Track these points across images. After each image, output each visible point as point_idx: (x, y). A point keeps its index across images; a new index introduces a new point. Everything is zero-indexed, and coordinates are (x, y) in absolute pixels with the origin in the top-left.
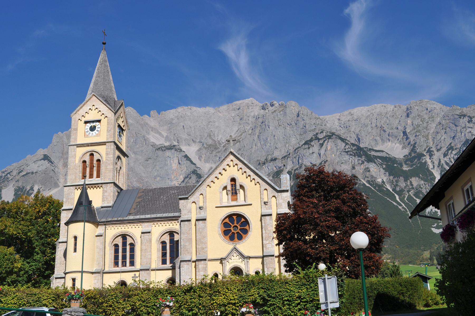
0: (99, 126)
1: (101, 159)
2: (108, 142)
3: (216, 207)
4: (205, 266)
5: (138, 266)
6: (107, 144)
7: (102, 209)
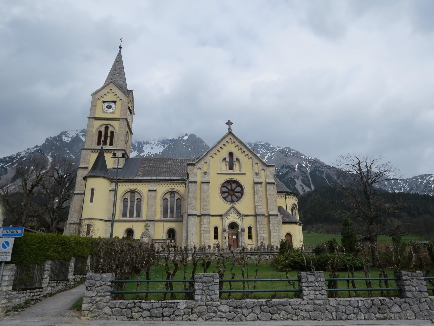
0: (114, 106)
1: (114, 130)
4: (209, 220)
5: (144, 217)
6: (121, 120)
7: (113, 170)
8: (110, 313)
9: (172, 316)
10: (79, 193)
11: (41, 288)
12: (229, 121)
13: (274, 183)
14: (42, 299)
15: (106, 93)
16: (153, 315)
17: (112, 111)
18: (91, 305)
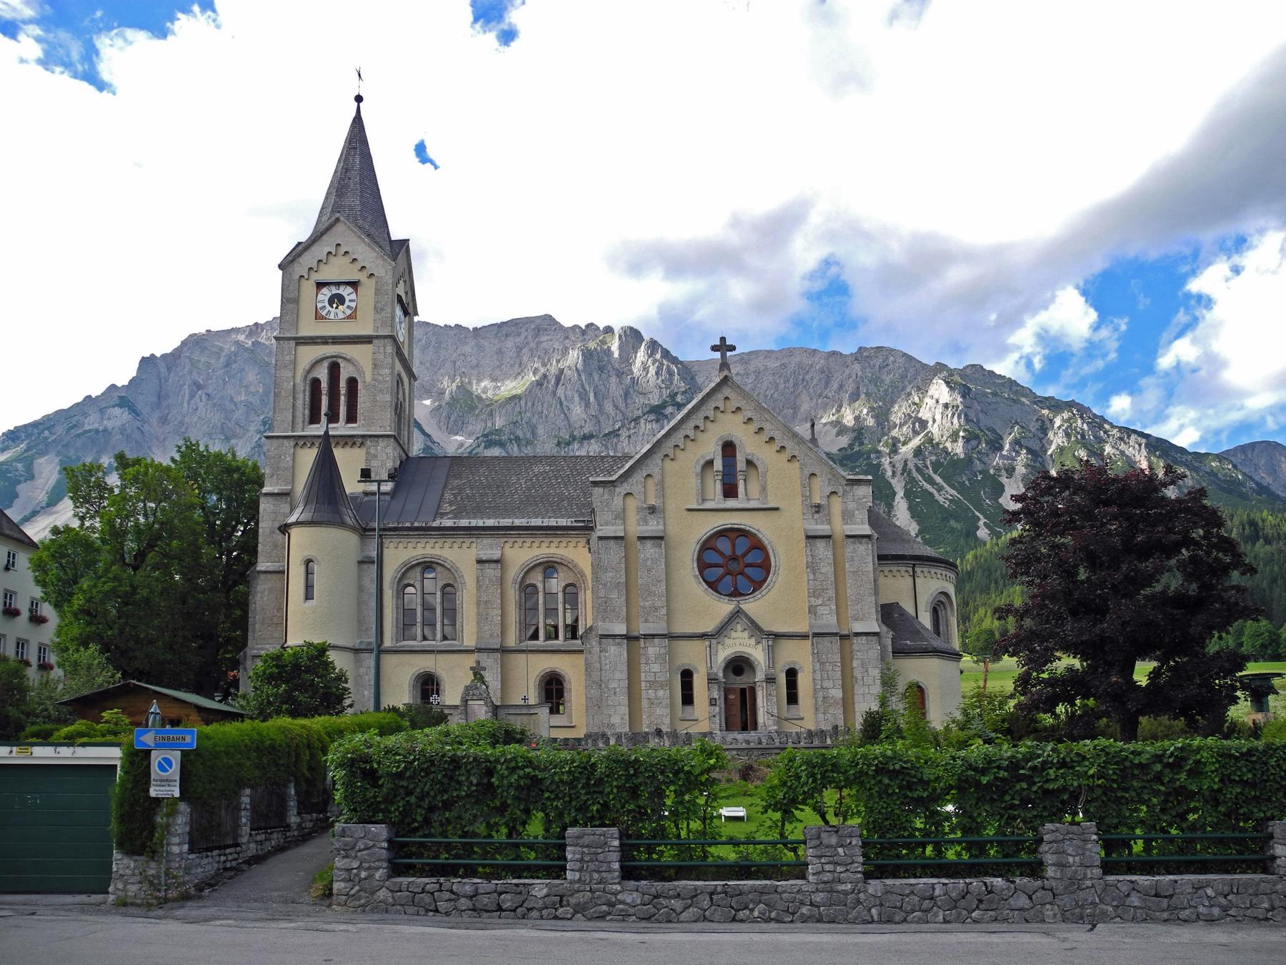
2: (377, 337)
3: (689, 510)
6: (375, 341)
8: (391, 900)
9: (519, 910)
10: (271, 569)
11: (238, 845)
12: (723, 339)
13: (868, 537)
14: (244, 867)
15: (323, 257)
16: (479, 906)
17: (349, 312)
18: (349, 885)
